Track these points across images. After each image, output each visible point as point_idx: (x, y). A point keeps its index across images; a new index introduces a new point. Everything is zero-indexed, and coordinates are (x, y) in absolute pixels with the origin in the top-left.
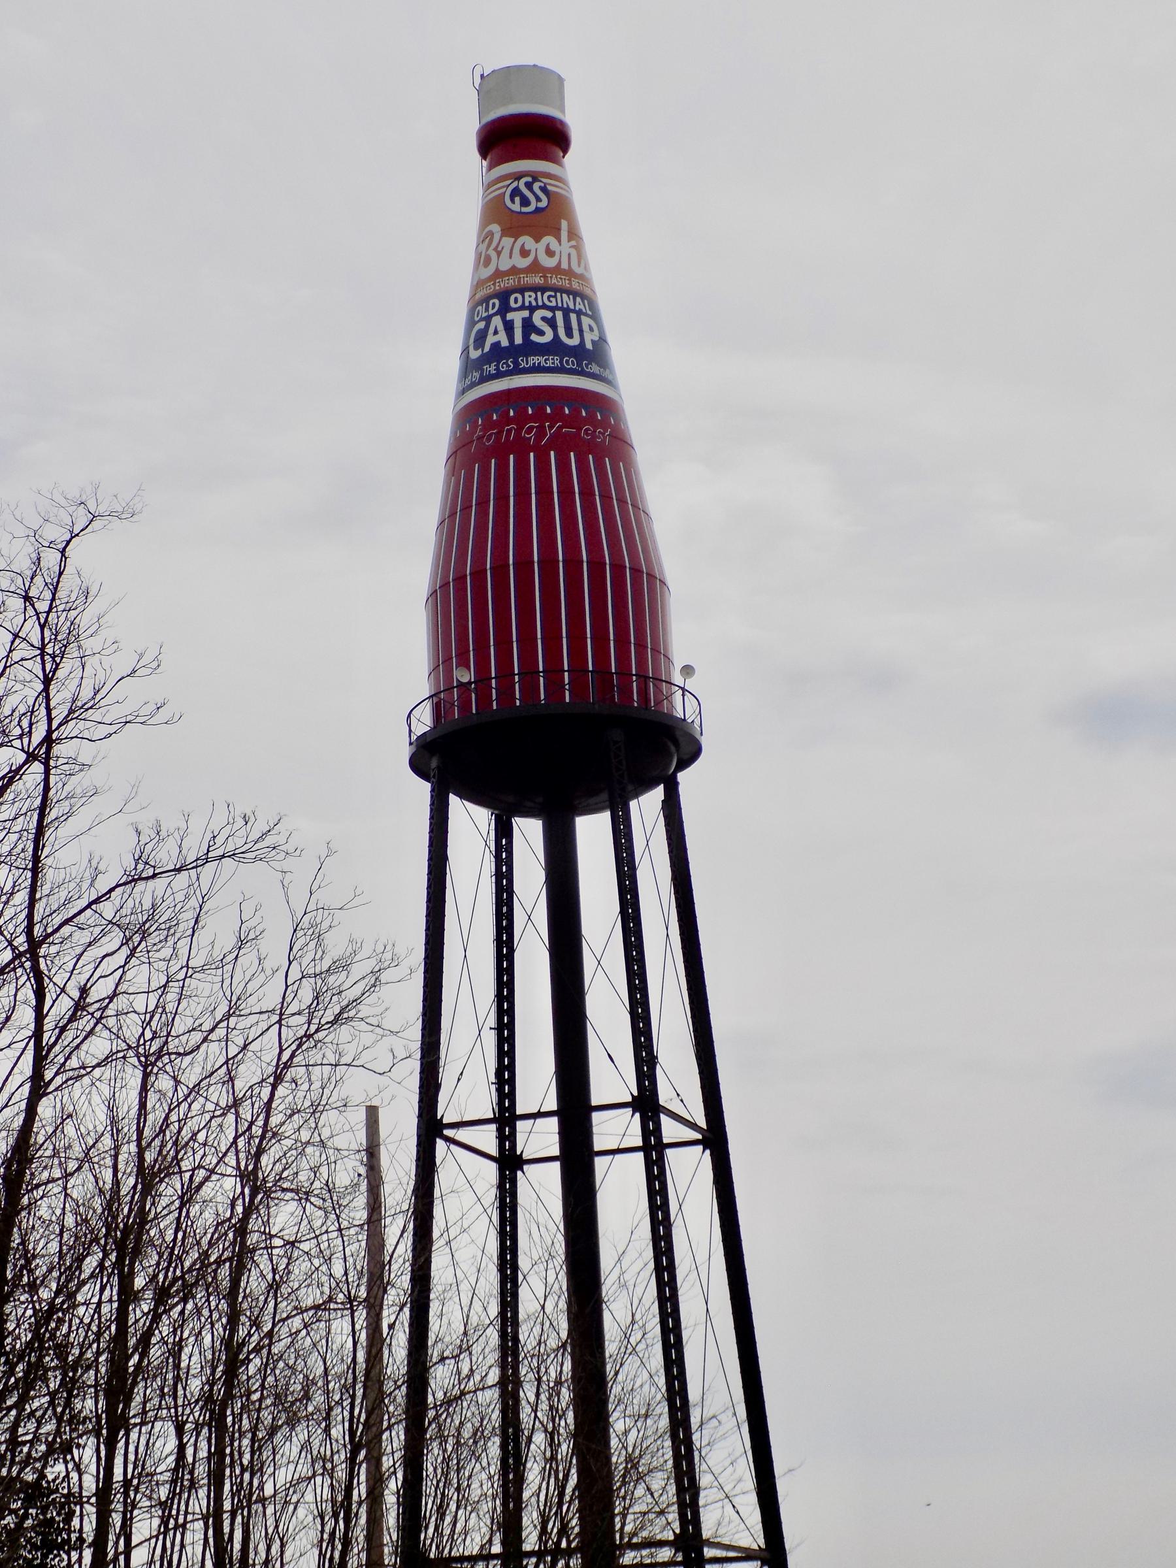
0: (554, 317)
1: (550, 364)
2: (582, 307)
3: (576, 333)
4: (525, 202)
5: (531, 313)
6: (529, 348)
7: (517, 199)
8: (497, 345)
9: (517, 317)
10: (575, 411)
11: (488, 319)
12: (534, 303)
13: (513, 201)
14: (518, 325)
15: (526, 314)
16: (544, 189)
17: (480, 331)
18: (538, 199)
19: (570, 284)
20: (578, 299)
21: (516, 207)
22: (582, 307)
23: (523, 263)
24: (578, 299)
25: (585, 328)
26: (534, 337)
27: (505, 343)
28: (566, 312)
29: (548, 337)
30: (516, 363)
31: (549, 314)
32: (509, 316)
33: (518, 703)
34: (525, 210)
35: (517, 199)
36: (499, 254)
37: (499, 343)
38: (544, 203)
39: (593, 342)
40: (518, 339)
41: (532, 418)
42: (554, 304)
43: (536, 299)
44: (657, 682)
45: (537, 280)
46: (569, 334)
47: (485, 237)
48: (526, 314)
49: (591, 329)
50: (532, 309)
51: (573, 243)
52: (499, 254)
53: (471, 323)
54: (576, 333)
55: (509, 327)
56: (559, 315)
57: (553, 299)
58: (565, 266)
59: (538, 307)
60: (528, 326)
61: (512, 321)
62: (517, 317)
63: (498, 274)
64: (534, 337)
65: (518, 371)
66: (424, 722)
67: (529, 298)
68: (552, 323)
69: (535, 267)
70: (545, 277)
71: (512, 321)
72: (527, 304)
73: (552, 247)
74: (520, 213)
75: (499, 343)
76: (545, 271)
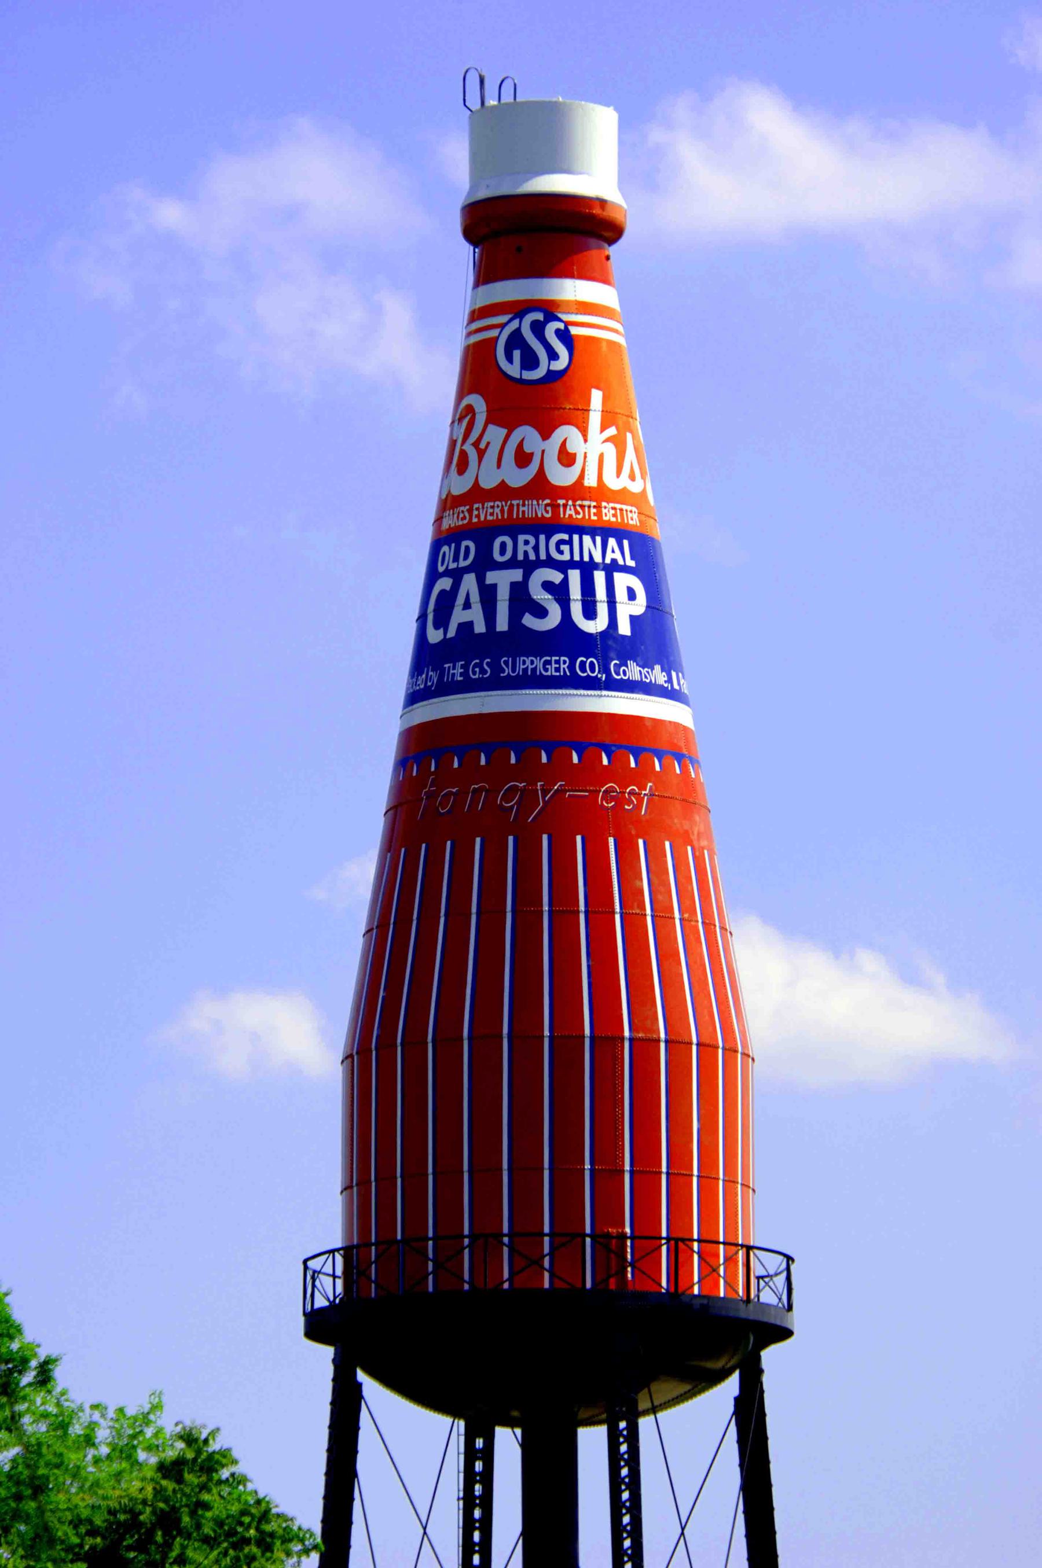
0: (565, 581)
1: (551, 672)
2: (618, 556)
3: (602, 609)
4: (530, 361)
5: (527, 576)
6: (522, 641)
7: (517, 354)
8: (466, 627)
9: (503, 580)
10: (589, 762)
11: (457, 575)
12: (532, 557)
13: (510, 359)
14: (503, 595)
15: (517, 575)
16: (564, 336)
17: (443, 592)
18: (553, 355)
19: (599, 514)
20: (612, 542)
21: (514, 370)
22: (618, 556)
23: (519, 478)
24: (612, 542)
25: (621, 595)
26: (529, 621)
27: (480, 628)
28: (587, 569)
29: (554, 618)
30: (496, 668)
31: (557, 577)
32: (491, 577)
33: (466, 1287)
34: (528, 375)
35: (517, 354)
36: (481, 454)
37: (470, 624)
38: (560, 364)
39: (633, 619)
40: (502, 624)
41: (515, 773)
42: (566, 557)
43: (536, 548)
44: (745, 1188)
45: (540, 509)
46: (590, 613)
47: (465, 415)
48: (517, 575)
49: (632, 595)
50: (529, 567)
51: (612, 431)
52: (481, 454)
53: (432, 576)
54: (602, 609)
55: (488, 594)
56: (575, 577)
57: (565, 548)
58: (590, 481)
59: (539, 564)
60: (520, 593)
61: (494, 586)
62: (503, 580)
63: (477, 494)
64: (529, 621)
65: (496, 683)
66: (329, 1289)
67: (525, 544)
68: (560, 592)
69: (540, 486)
70: (555, 507)
71: (494, 586)
72: (520, 557)
73: (570, 448)
74: (521, 381)
75: (470, 624)
76: (556, 492)
